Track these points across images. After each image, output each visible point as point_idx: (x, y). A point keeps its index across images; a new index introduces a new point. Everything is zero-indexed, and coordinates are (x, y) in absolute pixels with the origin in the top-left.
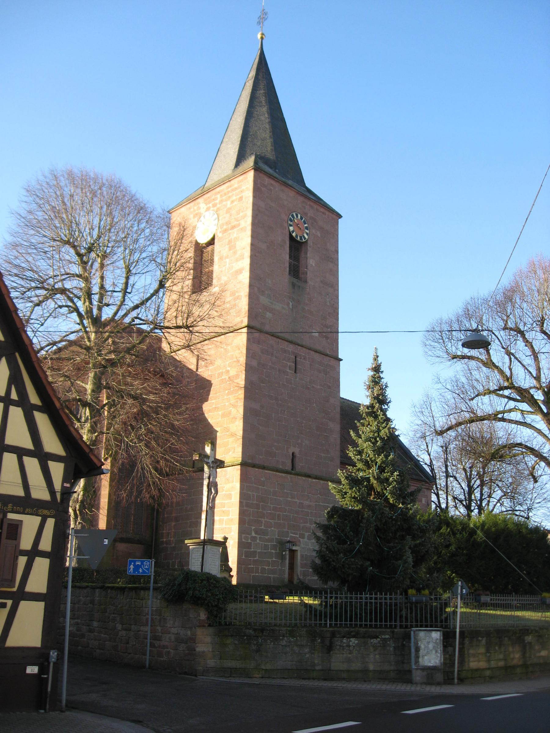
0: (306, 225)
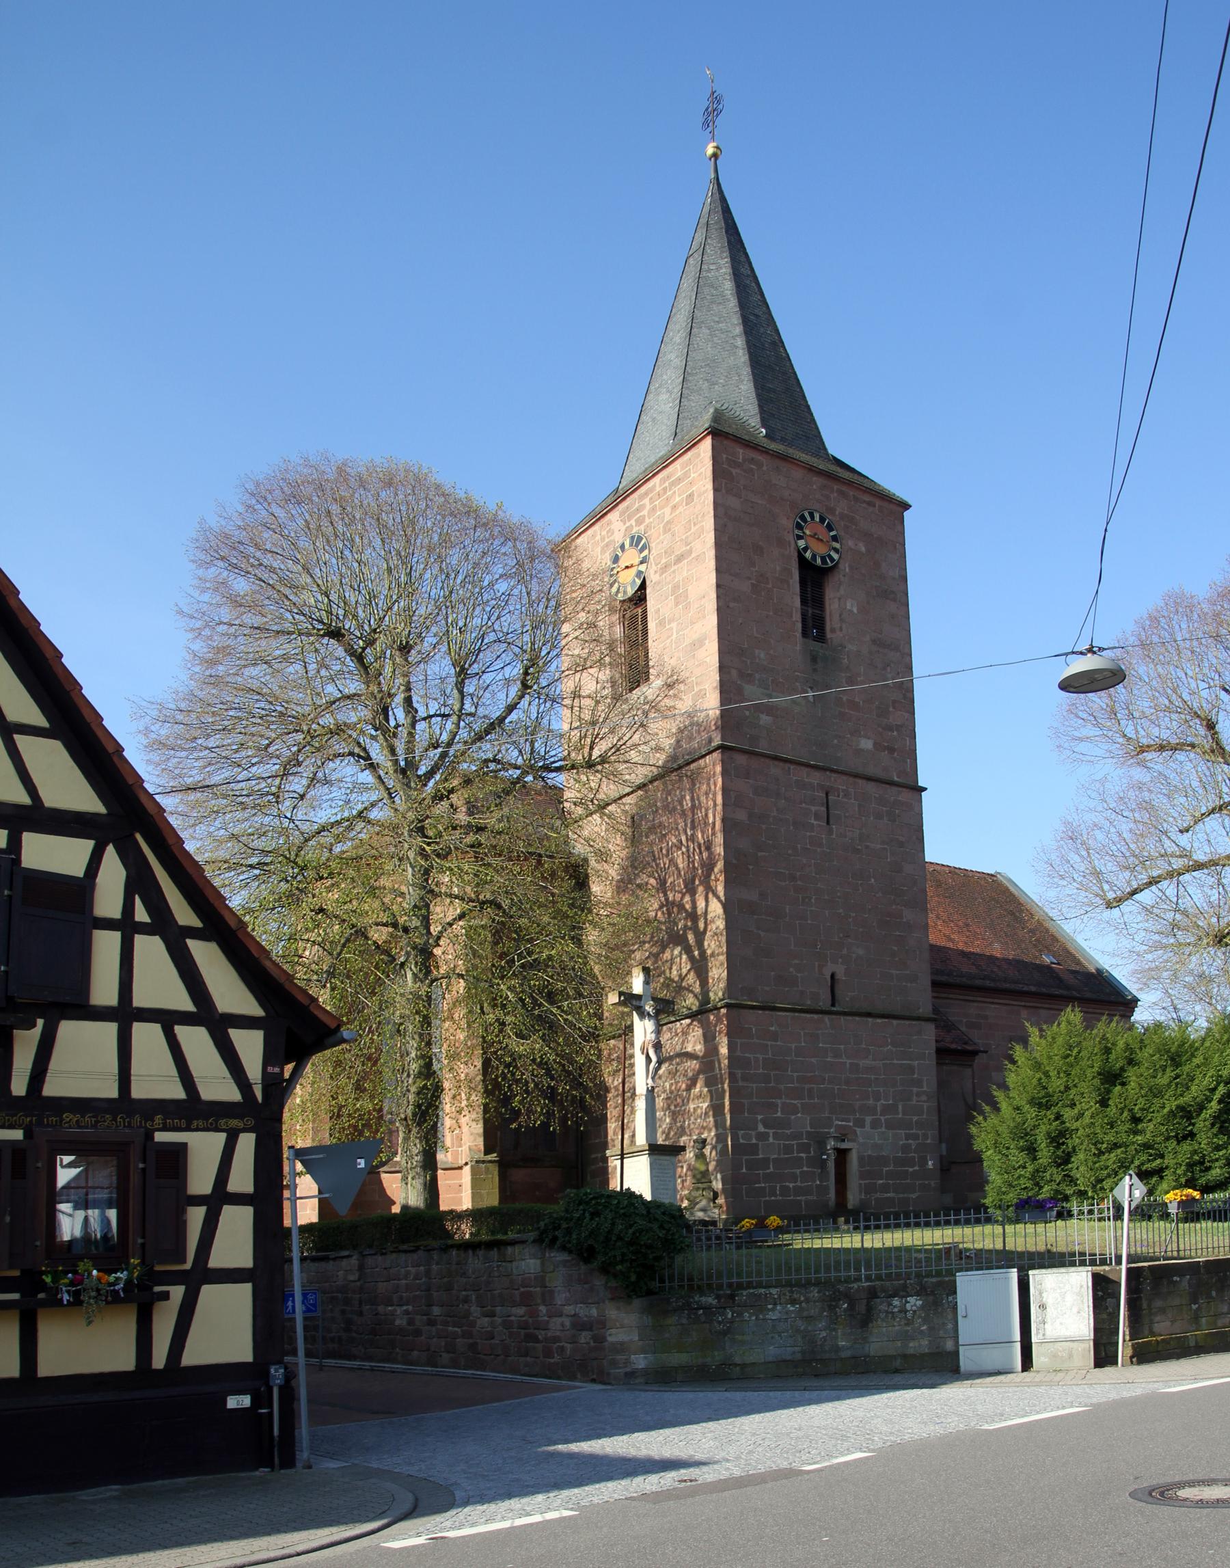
0: (832, 533)
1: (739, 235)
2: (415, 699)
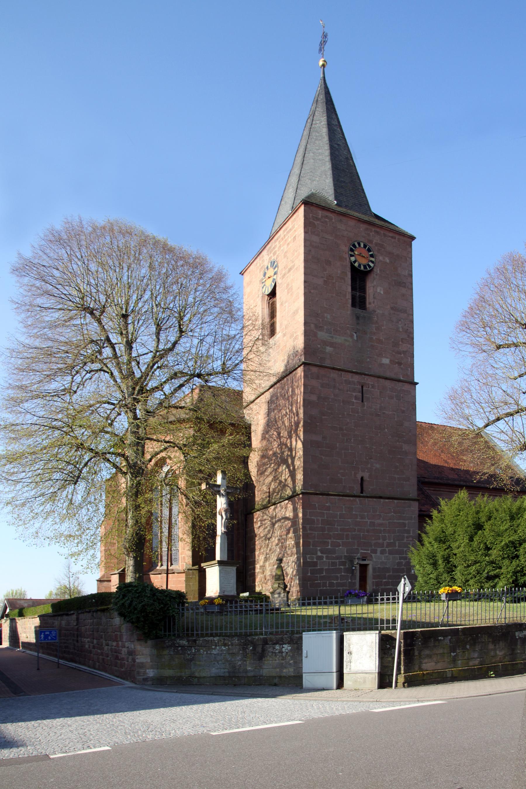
0: (370, 253)
2: (111, 336)
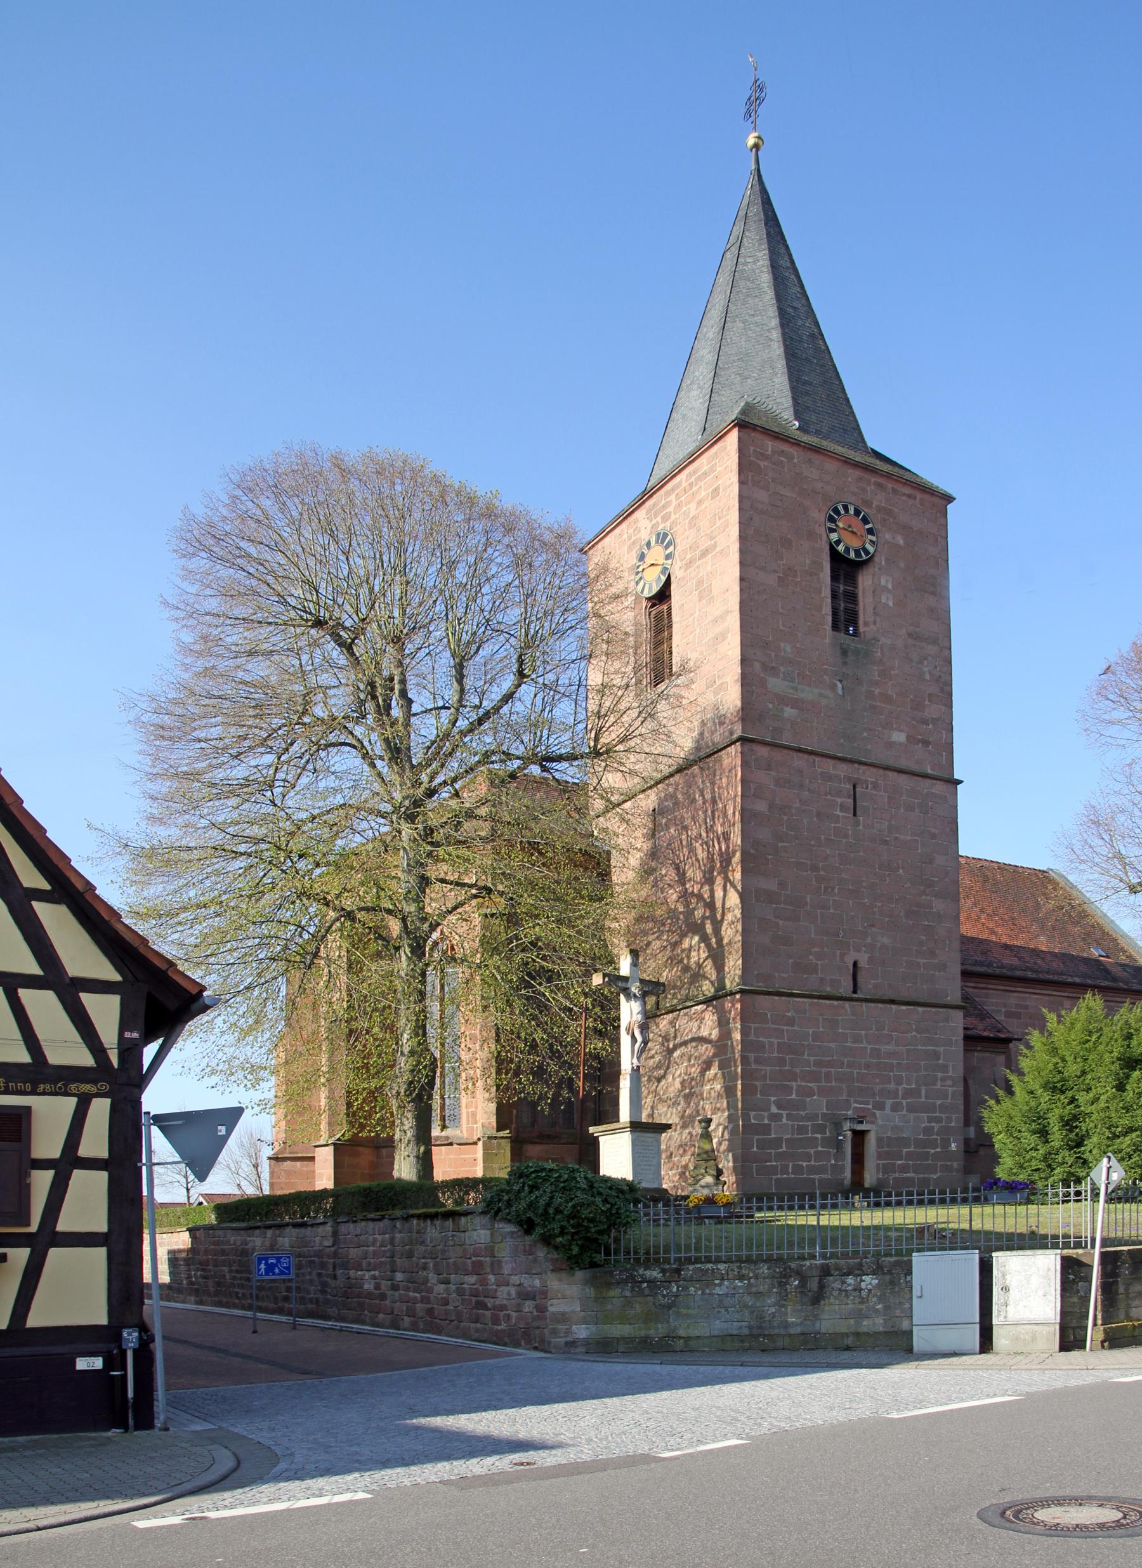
0: (867, 526)
1: (779, 226)
